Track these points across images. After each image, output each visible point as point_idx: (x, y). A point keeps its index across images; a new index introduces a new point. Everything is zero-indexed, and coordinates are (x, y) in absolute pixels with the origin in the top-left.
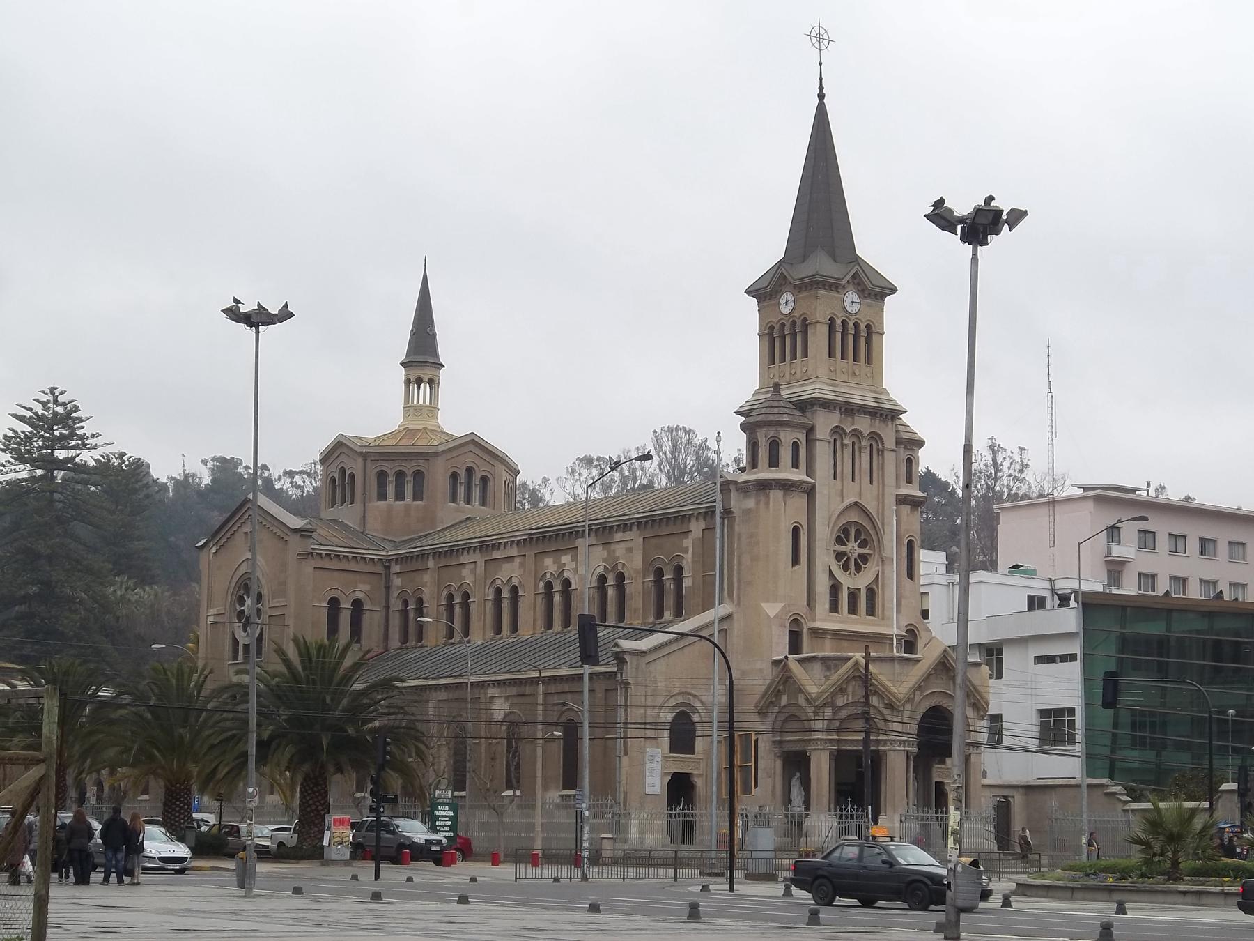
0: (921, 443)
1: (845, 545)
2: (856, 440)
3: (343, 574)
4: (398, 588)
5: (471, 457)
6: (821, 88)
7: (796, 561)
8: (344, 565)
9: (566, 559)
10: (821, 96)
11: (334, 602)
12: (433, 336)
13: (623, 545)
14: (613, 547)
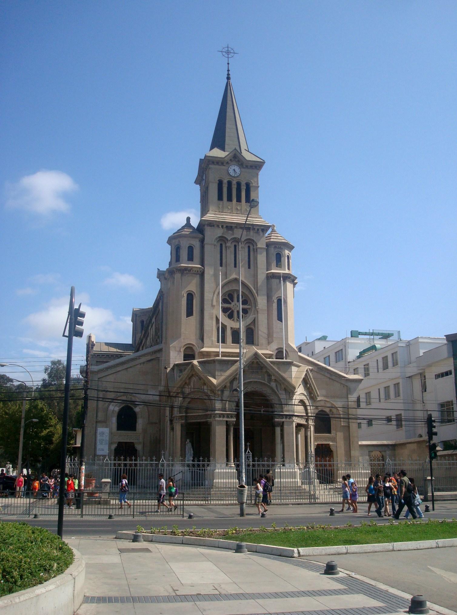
0: (291, 248)
1: (230, 303)
2: (222, 243)
6: (228, 74)
7: (190, 313)
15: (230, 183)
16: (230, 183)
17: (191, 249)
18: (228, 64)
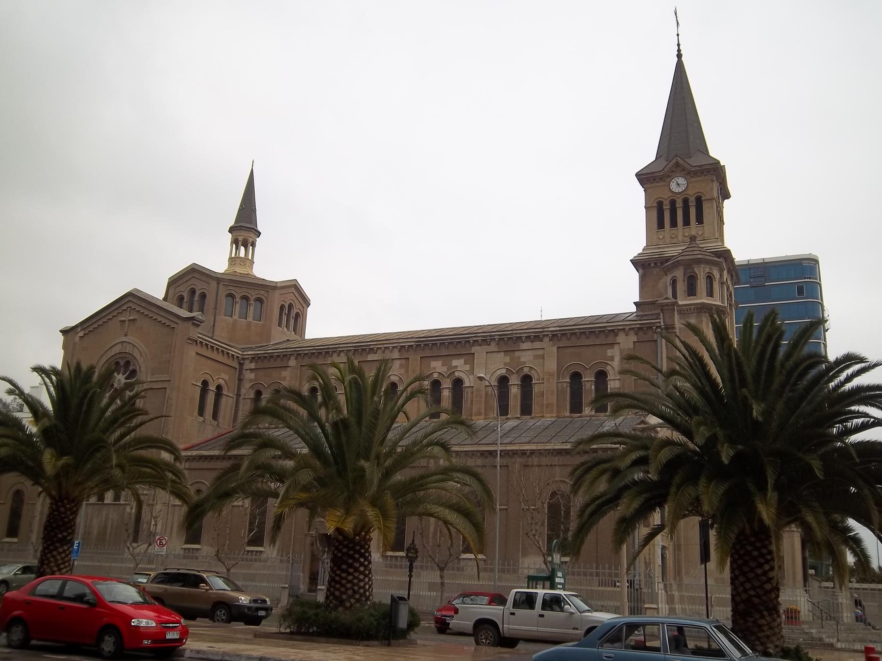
3: (213, 363)
4: (251, 380)
5: (291, 296)
6: (679, 51)
8: (214, 355)
9: (457, 363)
10: (679, 56)
11: (205, 383)
12: (254, 211)
13: (530, 353)
14: (517, 354)
15: (673, 203)
16: (673, 203)
17: (710, 278)
18: (678, 35)
